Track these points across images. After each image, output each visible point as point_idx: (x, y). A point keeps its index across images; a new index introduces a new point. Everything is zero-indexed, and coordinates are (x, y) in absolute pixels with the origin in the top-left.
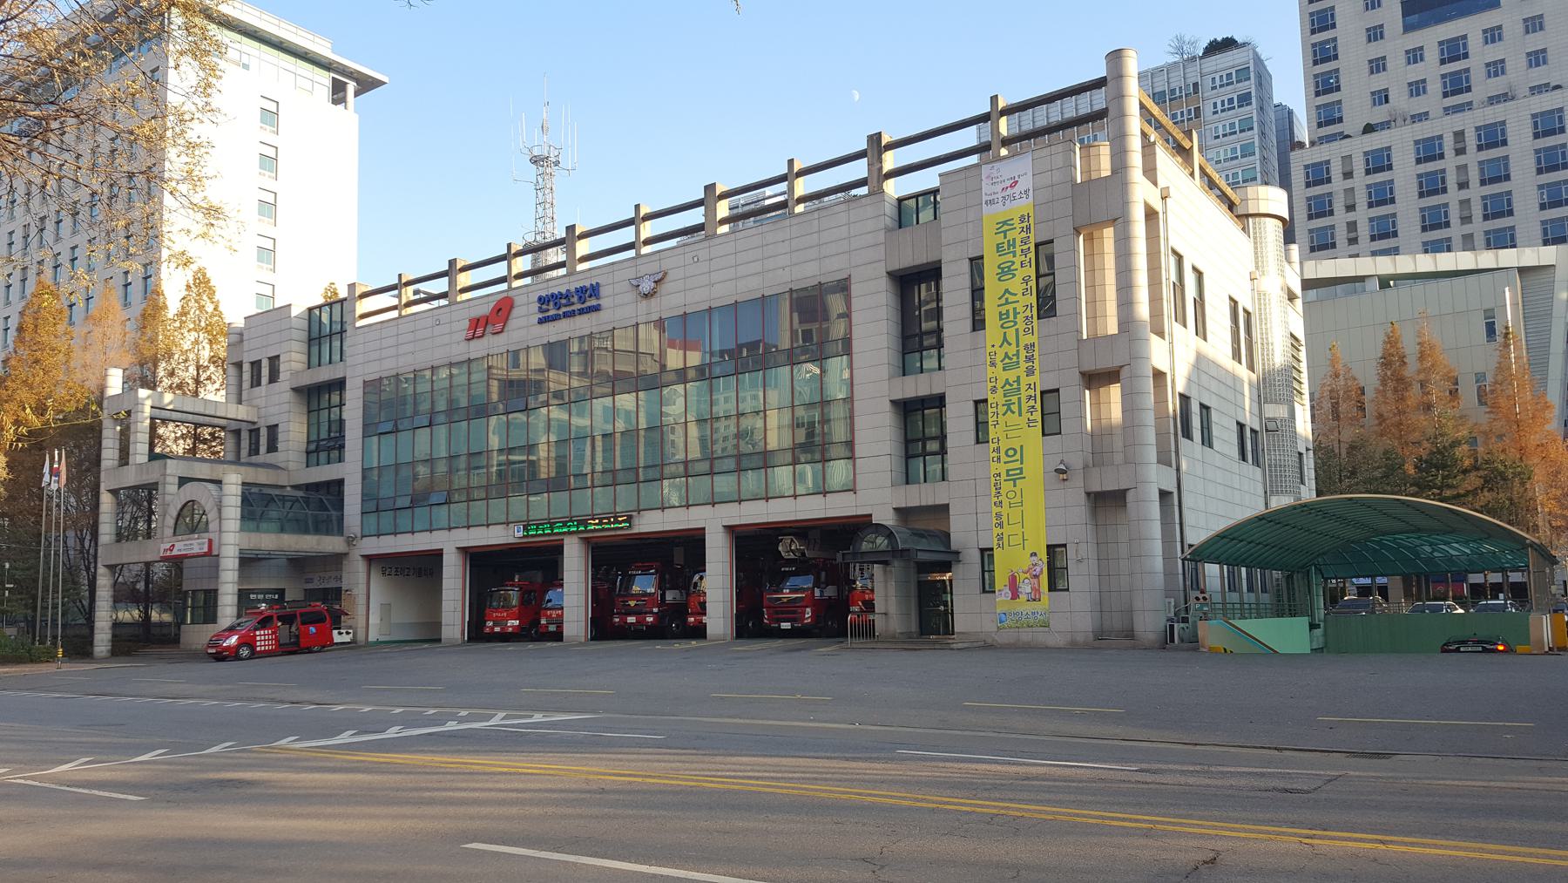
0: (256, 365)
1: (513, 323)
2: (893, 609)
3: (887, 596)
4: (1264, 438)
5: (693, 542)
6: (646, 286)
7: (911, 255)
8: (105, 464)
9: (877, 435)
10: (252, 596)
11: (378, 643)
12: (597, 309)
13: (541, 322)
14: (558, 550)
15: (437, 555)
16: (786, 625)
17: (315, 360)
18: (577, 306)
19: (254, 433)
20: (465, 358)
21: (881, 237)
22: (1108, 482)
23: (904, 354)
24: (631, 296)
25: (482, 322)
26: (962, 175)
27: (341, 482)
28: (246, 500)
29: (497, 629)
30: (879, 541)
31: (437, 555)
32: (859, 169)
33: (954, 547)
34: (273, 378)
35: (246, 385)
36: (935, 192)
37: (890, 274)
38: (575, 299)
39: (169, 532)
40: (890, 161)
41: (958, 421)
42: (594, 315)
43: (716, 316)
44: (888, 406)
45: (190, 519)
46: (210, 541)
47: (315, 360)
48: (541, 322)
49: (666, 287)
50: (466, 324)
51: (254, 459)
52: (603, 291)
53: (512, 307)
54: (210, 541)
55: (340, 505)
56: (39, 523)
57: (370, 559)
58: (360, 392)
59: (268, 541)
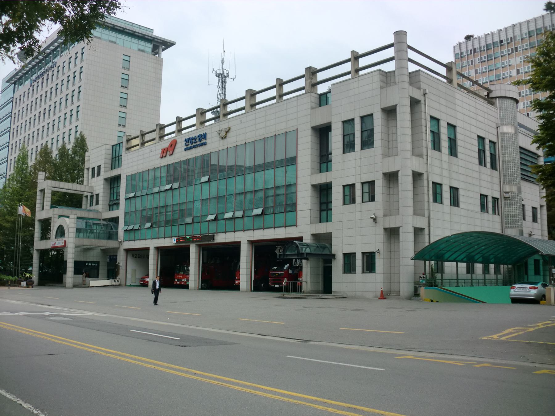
0: (93, 169)
1: (177, 150)
2: (309, 280)
3: (308, 272)
4: (502, 202)
5: (235, 247)
6: (223, 134)
7: (320, 121)
8: (37, 209)
9: (306, 200)
10: (87, 264)
11: (130, 286)
12: (205, 144)
13: (186, 150)
14: (188, 249)
15: (147, 249)
16: (277, 286)
17: (113, 166)
18: (199, 143)
19: (92, 197)
20: (159, 166)
21: (309, 111)
22: (392, 223)
23: (320, 164)
24: (218, 138)
25: (165, 151)
26: (339, 85)
27: (118, 218)
28: (292, 207)
29: (178, 283)
30: (53, 252)
31: (147, 249)
32: (347, 67)
33: (333, 252)
34: (99, 174)
35: (90, 177)
36: (394, 72)
37: (314, 128)
38: (197, 140)
39: (54, 237)
40: (363, 62)
41: (337, 195)
42: (204, 147)
43: (247, 146)
44: (310, 187)
45: (61, 232)
46: (65, 241)
47: (113, 166)
48: (186, 150)
49: (230, 134)
50: (160, 151)
51: (92, 208)
52: (208, 136)
53: (176, 143)
54: (65, 241)
55: (117, 227)
56: (97, 224)
57: (127, 251)
58: (50, 195)
59: (87, 242)
